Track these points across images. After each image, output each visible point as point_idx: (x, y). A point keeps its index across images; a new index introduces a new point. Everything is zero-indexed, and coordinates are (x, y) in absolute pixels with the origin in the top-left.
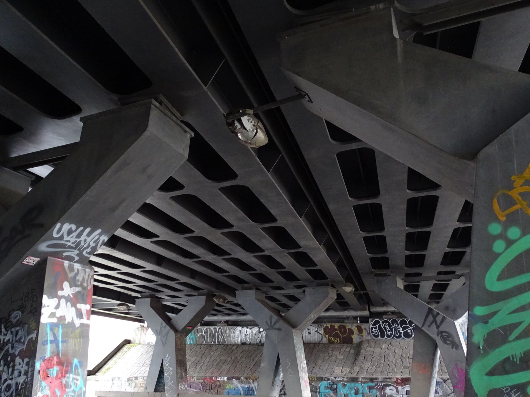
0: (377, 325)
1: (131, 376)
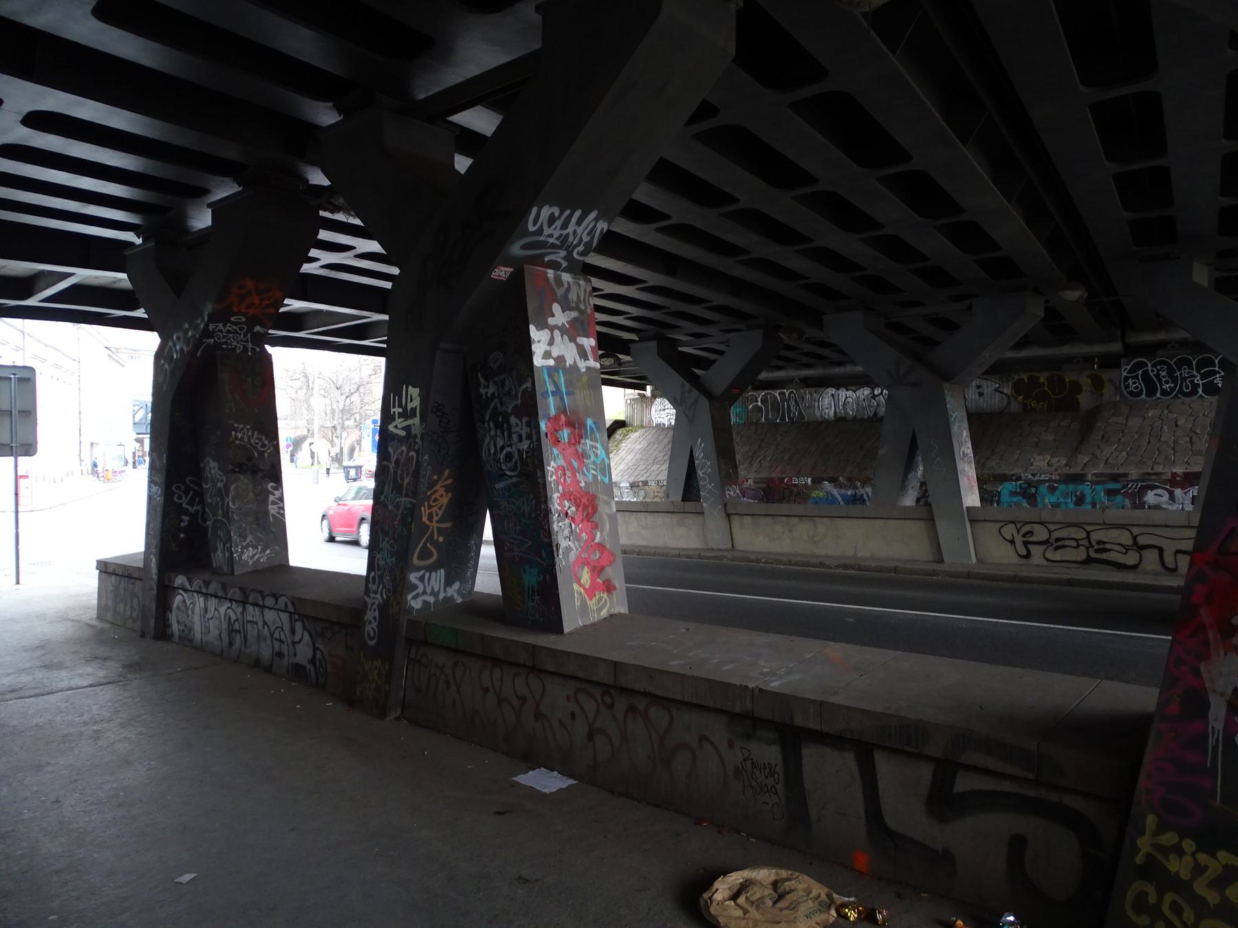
0: (1140, 372)
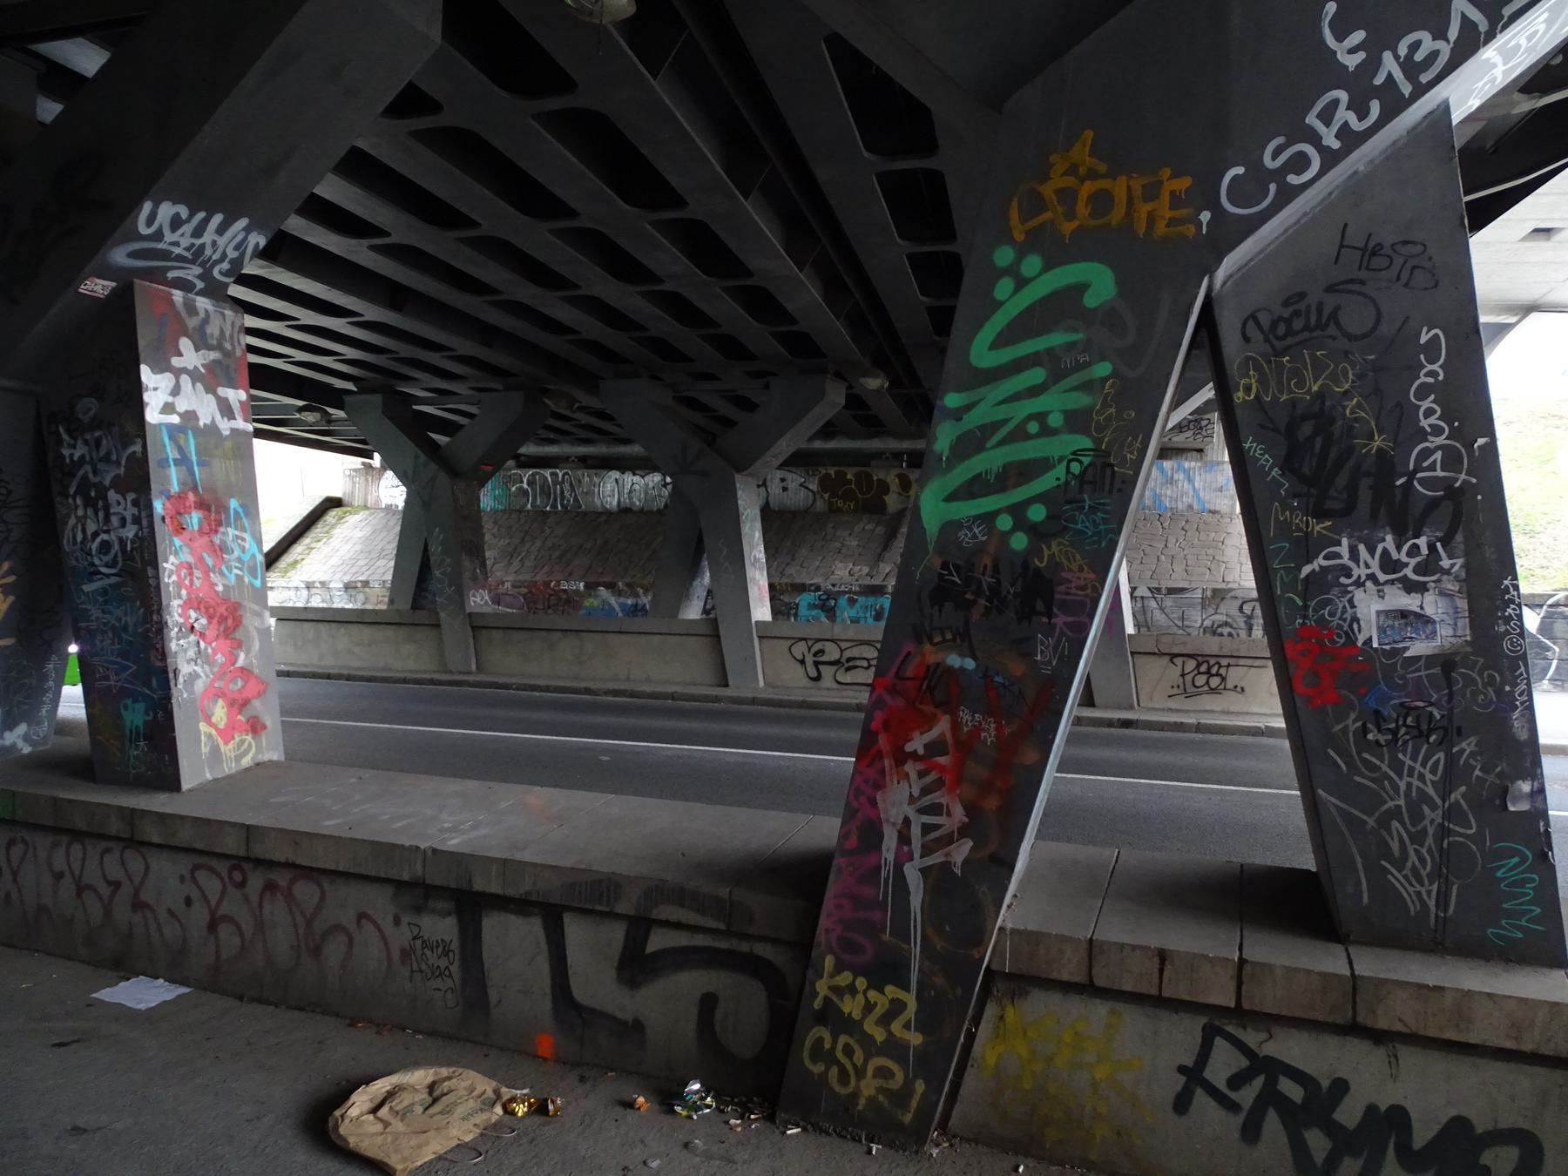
1: (353, 579)
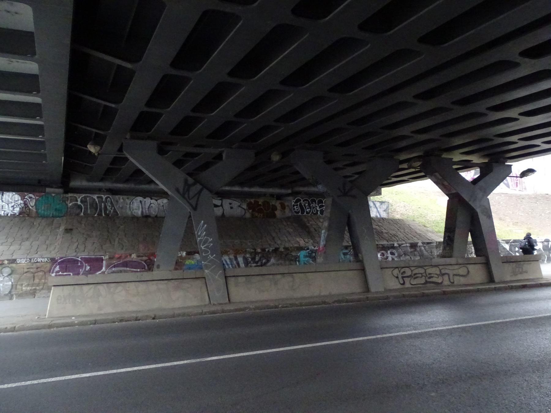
0: (299, 203)
